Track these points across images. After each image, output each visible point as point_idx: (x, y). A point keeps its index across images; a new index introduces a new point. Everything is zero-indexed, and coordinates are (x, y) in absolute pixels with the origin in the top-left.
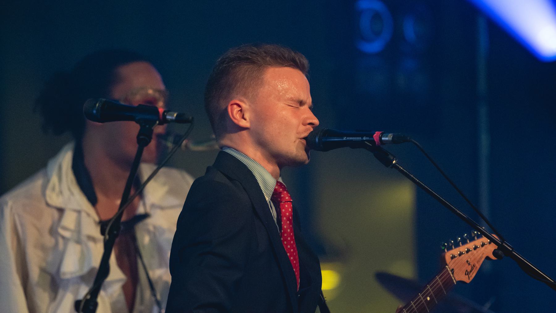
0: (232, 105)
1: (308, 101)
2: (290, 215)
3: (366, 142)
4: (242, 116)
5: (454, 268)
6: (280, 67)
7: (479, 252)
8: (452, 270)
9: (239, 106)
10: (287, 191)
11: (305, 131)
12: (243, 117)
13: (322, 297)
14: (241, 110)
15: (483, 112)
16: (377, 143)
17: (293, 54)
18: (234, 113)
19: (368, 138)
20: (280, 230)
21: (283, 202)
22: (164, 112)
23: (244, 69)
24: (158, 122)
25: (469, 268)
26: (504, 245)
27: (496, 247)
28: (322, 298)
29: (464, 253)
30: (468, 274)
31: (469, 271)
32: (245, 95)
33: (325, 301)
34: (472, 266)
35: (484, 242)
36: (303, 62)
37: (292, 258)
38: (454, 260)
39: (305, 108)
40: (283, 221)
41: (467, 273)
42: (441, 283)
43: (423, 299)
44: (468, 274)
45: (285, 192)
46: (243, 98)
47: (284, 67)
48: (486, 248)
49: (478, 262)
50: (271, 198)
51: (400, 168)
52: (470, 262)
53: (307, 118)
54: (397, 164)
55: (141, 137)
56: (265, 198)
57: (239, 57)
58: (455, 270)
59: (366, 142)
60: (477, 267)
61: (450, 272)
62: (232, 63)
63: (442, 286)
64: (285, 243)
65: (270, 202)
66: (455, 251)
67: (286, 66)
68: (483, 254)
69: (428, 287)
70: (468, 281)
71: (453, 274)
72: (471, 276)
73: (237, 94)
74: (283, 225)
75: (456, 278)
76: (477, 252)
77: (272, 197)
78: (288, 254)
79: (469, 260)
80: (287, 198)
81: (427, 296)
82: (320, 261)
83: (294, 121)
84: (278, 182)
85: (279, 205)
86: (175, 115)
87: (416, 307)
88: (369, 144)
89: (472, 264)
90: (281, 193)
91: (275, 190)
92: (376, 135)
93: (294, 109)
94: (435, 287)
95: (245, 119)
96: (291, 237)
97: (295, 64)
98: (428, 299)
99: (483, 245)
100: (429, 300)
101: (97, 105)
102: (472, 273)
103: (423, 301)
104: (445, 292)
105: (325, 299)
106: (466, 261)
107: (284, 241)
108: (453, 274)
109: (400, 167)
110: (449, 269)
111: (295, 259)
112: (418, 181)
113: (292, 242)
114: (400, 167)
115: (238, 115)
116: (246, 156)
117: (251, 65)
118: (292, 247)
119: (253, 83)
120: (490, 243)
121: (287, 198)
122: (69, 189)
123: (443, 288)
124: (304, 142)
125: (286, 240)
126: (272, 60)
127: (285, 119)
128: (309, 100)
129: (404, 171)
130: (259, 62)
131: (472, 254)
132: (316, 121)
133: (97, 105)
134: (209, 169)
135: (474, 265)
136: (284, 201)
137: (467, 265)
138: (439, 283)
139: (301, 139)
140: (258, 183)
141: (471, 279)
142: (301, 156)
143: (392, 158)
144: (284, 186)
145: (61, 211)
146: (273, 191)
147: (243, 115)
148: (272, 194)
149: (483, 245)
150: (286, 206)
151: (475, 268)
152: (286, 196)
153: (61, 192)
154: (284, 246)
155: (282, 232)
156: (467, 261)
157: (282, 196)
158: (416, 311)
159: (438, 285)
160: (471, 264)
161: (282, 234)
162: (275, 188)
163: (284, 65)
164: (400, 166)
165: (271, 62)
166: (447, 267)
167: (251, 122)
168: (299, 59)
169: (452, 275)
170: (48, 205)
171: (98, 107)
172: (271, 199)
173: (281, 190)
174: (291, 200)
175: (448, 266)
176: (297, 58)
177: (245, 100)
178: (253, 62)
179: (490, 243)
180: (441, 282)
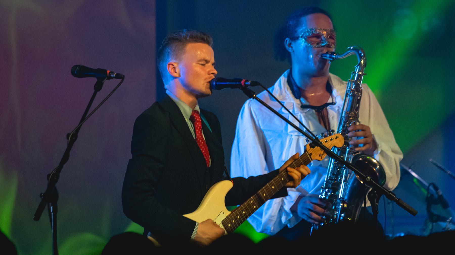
0: (169, 65)
1: (211, 61)
5: (312, 153)
7: (329, 143)
9: (173, 65)
11: (210, 78)
22: (110, 72)
24: (106, 78)
30: (321, 156)
31: (322, 154)
37: (203, 151)
43: (266, 190)
44: (321, 156)
47: (198, 43)
54: (256, 97)
55: (96, 86)
72: (323, 157)
78: (201, 149)
80: (198, 120)
81: (282, 177)
83: (202, 73)
94: (298, 163)
102: (323, 155)
104: (287, 181)
107: (198, 142)
124: (209, 84)
125: (200, 142)
128: (213, 60)
132: (216, 72)
143: (253, 94)
147: (175, 71)
150: (198, 124)
154: (199, 145)
159: (300, 162)
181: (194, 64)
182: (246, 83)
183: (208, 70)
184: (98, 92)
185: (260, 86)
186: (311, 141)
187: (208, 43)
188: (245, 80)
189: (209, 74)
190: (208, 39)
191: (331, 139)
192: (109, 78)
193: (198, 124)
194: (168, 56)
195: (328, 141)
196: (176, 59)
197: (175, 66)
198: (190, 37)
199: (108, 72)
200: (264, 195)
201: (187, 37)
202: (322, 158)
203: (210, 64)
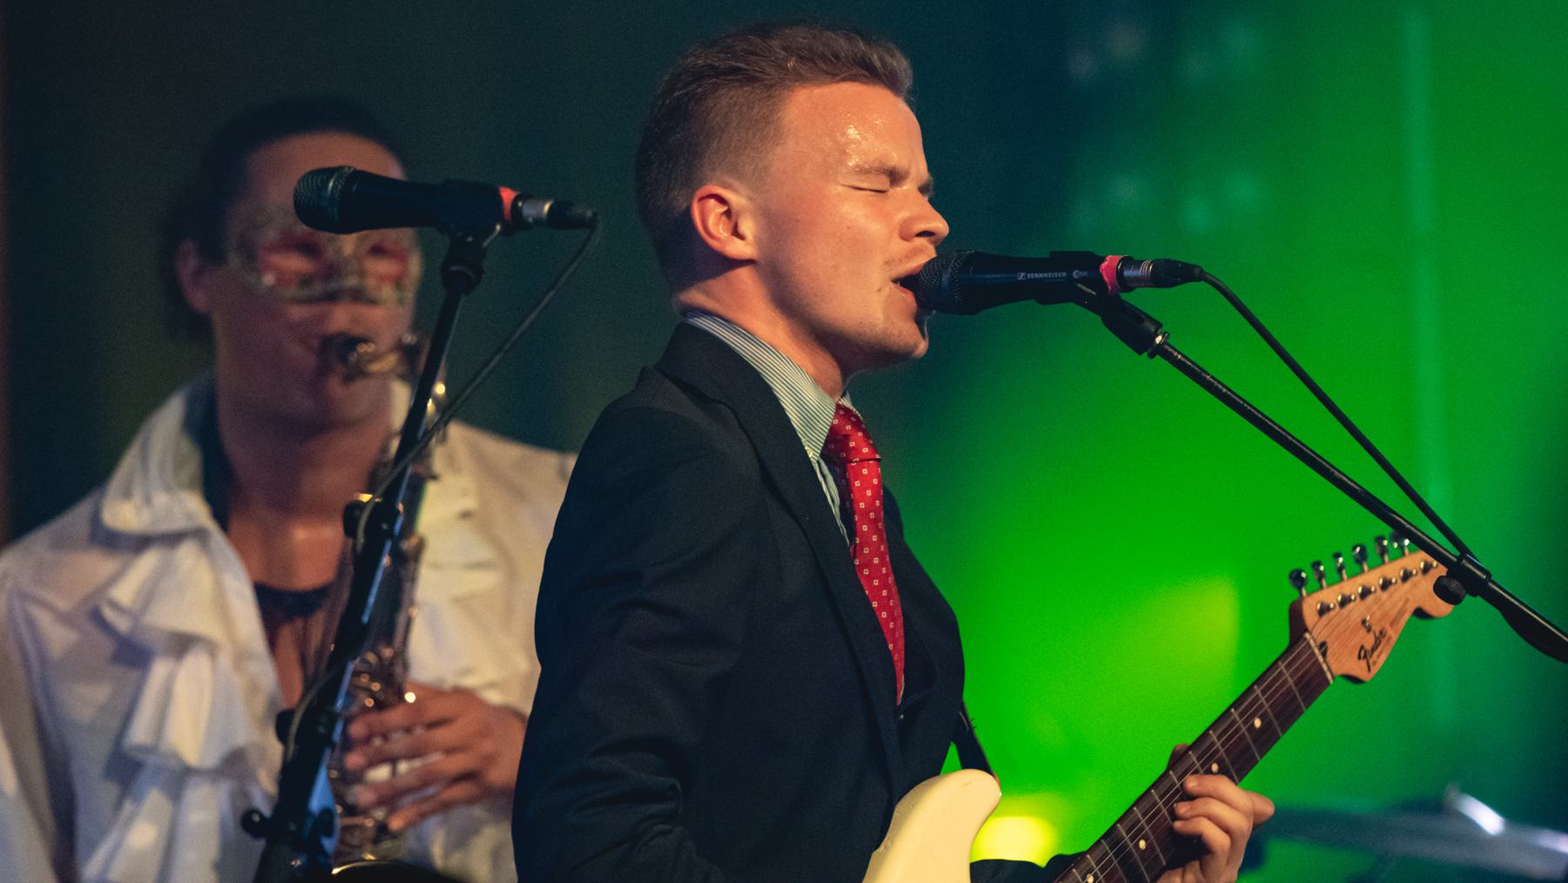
0: (701, 199)
1: (913, 171)
2: (874, 497)
3: (1079, 285)
5: (1328, 641)
7: (1397, 595)
8: (1323, 646)
9: (722, 200)
10: (864, 431)
12: (736, 233)
13: (963, 718)
14: (728, 214)
16: (1110, 287)
17: (862, 46)
18: (711, 222)
19: (1085, 274)
20: (852, 539)
22: (516, 199)
23: (729, 99)
25: (1369, 641)
26: (1463, 566)
29: (1353, 597)
31: (1368, 647)
32: (735, 171)
34: (1377, 633)
35: (1410, 568)
36: (892, 65)
37: (884, 615)
38: (1326, 618)
39: (909, 187)
40: (858, 535)
41: (1364, 654)
42: (1291, 681)
44: (1365, 657)
45: (860, 434)
46: (730, 180)
47: (838, 82)
48: (1415, 585)
50: (822, 451)
51: (1177, 357)
53: (919, 218)
56: (805, 452)
57: (712, 67)
58: (1329, 644)
59: (1079, 285)
60: (1390, 638)
61: (1316, 651)
62: (694, 86)
63: (1294, 688)
65: (818, 462)
67: (844, 80)
68: (1407, 601)
71: (1324, 655)
72: (1375, 663)
73: (714, 170)
74: (858, 524)
76: (1390, 596)
77: (823, 448)
78: (875, 604)
79: (1368, 618)
81: (1253, 716)
84: (839, 407)
85: (845, 471)
86: (547, 207)
87: (1223, 745)
88: (1089, 290)
89: (1376, 628)
90: (847, 437)
91: (833, 429)
92: (1108, 266)
93: (871, 196)
94: (1276, 691)
95: (742, 237)
97: (869, 73)
98: (1258, 723)
100: (1260, 728)
101: (331, 184)
102: (1376, 654)
106: (1359, 620)
107: (862, 567)
108: (1324, 655)
109: (1176, 354)
110: (1312, 642)
111: (891, 617)
113: (884, 570)
115: (721, 226)
116: (749, 335)
119: (754, 137)
121: (865, 450)
123: (1297, 694)
125: (868, 564)
127: (849, 228)
128: (919, 169)
131: (1377, 601)
132: (940, 225)
133: (331, 184)
134: (643, 376)
135: (1381, 632)
136: (858, 460)
137: (1363, 631)
142: (898, 337)
143: (1153, 330)
144: (856, 416)
149: (1407, 576)
151: (1384, 641)
152: (864, 444)
155: (856, 544)
156: (1364, 622)
157: (852, 444)
158: (1224, 756)
160: (1373, 627)
161: (857, 551)
167: (759, 242)
168: (881, 59)
169: (1321, 659)
171: (332, 191)
172: (822, 455)
174: (878, 457)
175: (1310, 633)
176: (876, 56)
177: (736, 184)
178: (751, 80)
180: (1292, 678)
182: (1127, 273)
183: (903, 215)
184: (1033, 300)
186: (1440, 570)
187: (889, 80)
189: (905, 237)
190: (889, 59)
193: (865, 471)
199: (1110, 263)
200: (1142, 844)
202: (1369, 670)
203: (909, 187)
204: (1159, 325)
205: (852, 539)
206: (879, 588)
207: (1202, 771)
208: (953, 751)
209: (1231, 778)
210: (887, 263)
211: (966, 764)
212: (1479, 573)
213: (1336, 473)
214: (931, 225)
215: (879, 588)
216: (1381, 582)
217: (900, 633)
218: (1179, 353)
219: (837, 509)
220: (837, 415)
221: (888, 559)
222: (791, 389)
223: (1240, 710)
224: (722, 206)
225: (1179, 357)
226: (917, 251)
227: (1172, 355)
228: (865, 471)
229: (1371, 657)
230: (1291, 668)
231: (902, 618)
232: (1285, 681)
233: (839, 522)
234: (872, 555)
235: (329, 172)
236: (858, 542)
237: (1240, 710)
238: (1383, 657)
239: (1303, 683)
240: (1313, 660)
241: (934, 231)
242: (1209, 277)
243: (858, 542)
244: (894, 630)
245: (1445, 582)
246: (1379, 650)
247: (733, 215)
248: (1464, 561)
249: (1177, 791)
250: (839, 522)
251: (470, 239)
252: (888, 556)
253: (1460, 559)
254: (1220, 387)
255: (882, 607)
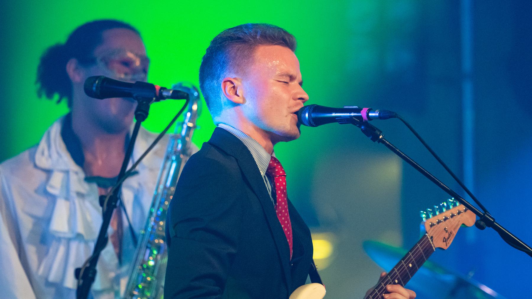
1: (298, 77)
3: (354, 118)
4: (235, 93)
6: (270, 45)
7: (456, 219)
8: (432, 237)
9: (232, 83)
12: (236, 94)
13: (313, 265)
15: (468, 89)
20: (275, 203)
21: (278, 176)
24: (154, 99)
25: (447, 236)
26: (486, 217)
27: (479, 218)
28: (313, 266)
30: (445, 241)
31: (446, 238)
33: (316, 269)
34: (449, 233)
35: (460, 210)
38: (433, 227)
41: (445, 240)
42: (422, 251)
47: (274, 45)
48: (462, 216)
49: (455, 229)
50: (266, 173)
52: (448, 230)
53: (299, 93)
54: (383, 139)
55: (139, 113)
59: (354, 118)
61: (430, 240)
63: (423, 253)
64: (280, 215)
65: (265, 177)
66: (433, 219)
67: (276, 44)
68: (459, 221)
69: (410, 254)
70: (445, 248)
72: (448, 243)
73: (222, 67)
75: (435, 246)
77: (266, 171)
78: (283, 226)
79: (447, 228)
82: (311, 231)
89: (449, 231)
90: (275, 168)
91: (270, 165)
94: (417, 254)
95: (238, 96)
96: (285, 209)
98: (410, 265)
99: (459, 213)
101: (97, 82)
102: (449, 240)
103: (406, 268)
105: (317, 267)
106: (444, 228)
107: (279, 213)
108: (432, 241)
109: (387, 142)
110: (429, 237)
111: (288, 230)
112: (403, 155)
113: (286, 214)
114: (387, 142)
115: (231, 91)
117: (242, 44)
118: (286, 219)
120: (465, 211)
122: (58, 153)
125: (281, 212)
126: (263, 39)
127: (276, 95)
129: (390, 145)
130: (251, 41)
133: (97, 82)
135: (451, 233)
136: (278, 175)
138: (420, 250)
139: (292, 113)
140: (253, 158)
141: (449, 245)
143: (379, 133)
145: (49, 172)
146: (268, 166)
147: (236, 92)
148: (267, 169)
149: (459, 213)
151: (451, 235)
153: (50, 156)
160: (448, 231)
161: (277, 207)
162: (270, 163)
163: (274, 44)
164: (387, 141)
165: (261, 41)
166: (427, 234)
169: (431, 243)
170: (36, 166)
172: (266, 174)
173: (275, 164)
175: (428, 234)
179: (465, 211)
181: (272, 81)
182: (370, 114)
185: (396, 118)
188: (368, 109)
189: (295, 99)
191: (452, 214)
192: (160, 97)
194: (223, 68)
195: (430, 222)
196: (237, 73)
197: (235, 85)
198: (262, 36)
201: (256, 36)
202: (447, 246)
204: (381, 132)
205: (275, 203)
206: (284, 220)
207: (392, 283)
208: (309, 278)
209: (402, 285)
210: (289, 108)
211: (313, 281)
212: (491, 219)
213: (442, 184)
214: (303, 96)
215: (284, 220)
216: (451, 215)
217: (291, 236)
218: (388, 142)
219: (271, 193)
220: (271, 160)
221: (288, 210)
222: (257, 151)
223: (405, 261)
224: (232, 84)
225: (388, 143)
226: (297, 104)
227: (385, 142)
228: (281, 180)
229: (447, 241)
230: (422, 246)
231: (292, 230)
232: (420, 251)
233: (271, 197)
234: (282, 209)
235: (97, 78)
236: (277, 205)
237: (405, 261)
238: (451, 241)
239: (424, 248)
240: (429, 243)
241: (304, 98)
242: (399, 116)
243: (277, 205)
244: (289, 234)
245: (479, 222)
246: (450, 238)
247: (235, 88)
248: (486, 215)
249: (384, 290)
250: (271, 197)
251: (144, 103)
252: (288, 209)
253: (484, 214)
254: (402, 153)
255: (285, 227)
